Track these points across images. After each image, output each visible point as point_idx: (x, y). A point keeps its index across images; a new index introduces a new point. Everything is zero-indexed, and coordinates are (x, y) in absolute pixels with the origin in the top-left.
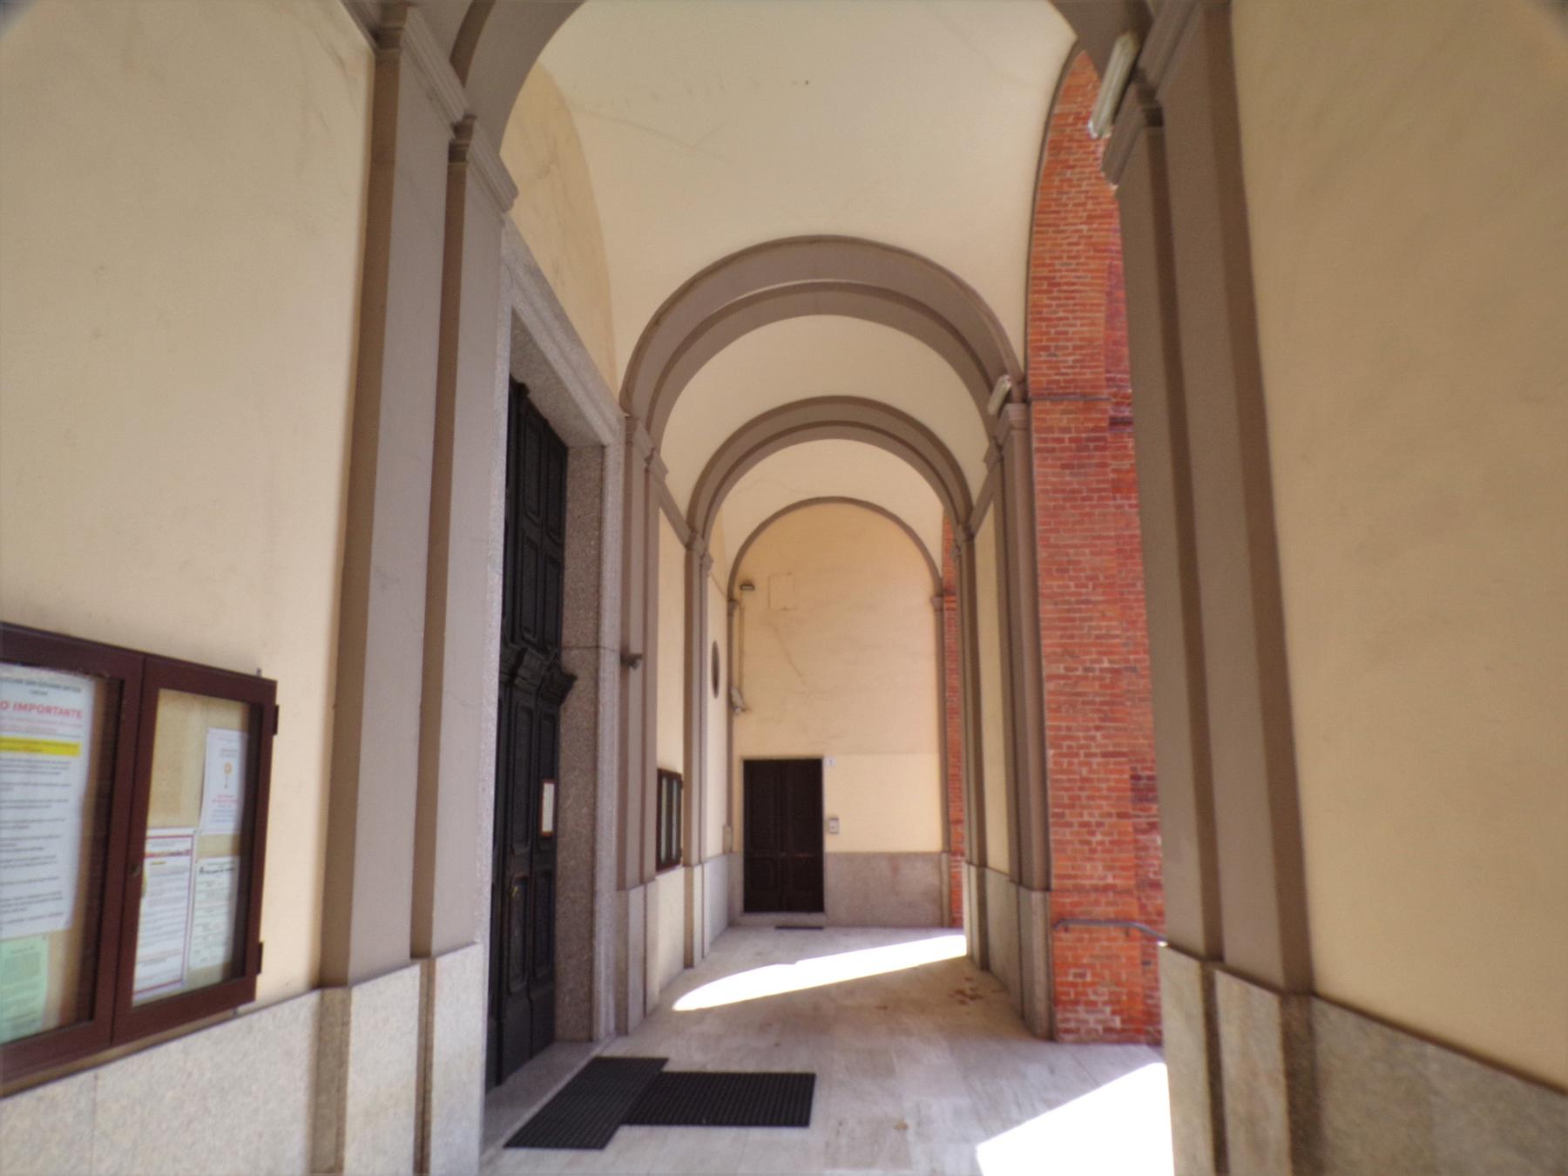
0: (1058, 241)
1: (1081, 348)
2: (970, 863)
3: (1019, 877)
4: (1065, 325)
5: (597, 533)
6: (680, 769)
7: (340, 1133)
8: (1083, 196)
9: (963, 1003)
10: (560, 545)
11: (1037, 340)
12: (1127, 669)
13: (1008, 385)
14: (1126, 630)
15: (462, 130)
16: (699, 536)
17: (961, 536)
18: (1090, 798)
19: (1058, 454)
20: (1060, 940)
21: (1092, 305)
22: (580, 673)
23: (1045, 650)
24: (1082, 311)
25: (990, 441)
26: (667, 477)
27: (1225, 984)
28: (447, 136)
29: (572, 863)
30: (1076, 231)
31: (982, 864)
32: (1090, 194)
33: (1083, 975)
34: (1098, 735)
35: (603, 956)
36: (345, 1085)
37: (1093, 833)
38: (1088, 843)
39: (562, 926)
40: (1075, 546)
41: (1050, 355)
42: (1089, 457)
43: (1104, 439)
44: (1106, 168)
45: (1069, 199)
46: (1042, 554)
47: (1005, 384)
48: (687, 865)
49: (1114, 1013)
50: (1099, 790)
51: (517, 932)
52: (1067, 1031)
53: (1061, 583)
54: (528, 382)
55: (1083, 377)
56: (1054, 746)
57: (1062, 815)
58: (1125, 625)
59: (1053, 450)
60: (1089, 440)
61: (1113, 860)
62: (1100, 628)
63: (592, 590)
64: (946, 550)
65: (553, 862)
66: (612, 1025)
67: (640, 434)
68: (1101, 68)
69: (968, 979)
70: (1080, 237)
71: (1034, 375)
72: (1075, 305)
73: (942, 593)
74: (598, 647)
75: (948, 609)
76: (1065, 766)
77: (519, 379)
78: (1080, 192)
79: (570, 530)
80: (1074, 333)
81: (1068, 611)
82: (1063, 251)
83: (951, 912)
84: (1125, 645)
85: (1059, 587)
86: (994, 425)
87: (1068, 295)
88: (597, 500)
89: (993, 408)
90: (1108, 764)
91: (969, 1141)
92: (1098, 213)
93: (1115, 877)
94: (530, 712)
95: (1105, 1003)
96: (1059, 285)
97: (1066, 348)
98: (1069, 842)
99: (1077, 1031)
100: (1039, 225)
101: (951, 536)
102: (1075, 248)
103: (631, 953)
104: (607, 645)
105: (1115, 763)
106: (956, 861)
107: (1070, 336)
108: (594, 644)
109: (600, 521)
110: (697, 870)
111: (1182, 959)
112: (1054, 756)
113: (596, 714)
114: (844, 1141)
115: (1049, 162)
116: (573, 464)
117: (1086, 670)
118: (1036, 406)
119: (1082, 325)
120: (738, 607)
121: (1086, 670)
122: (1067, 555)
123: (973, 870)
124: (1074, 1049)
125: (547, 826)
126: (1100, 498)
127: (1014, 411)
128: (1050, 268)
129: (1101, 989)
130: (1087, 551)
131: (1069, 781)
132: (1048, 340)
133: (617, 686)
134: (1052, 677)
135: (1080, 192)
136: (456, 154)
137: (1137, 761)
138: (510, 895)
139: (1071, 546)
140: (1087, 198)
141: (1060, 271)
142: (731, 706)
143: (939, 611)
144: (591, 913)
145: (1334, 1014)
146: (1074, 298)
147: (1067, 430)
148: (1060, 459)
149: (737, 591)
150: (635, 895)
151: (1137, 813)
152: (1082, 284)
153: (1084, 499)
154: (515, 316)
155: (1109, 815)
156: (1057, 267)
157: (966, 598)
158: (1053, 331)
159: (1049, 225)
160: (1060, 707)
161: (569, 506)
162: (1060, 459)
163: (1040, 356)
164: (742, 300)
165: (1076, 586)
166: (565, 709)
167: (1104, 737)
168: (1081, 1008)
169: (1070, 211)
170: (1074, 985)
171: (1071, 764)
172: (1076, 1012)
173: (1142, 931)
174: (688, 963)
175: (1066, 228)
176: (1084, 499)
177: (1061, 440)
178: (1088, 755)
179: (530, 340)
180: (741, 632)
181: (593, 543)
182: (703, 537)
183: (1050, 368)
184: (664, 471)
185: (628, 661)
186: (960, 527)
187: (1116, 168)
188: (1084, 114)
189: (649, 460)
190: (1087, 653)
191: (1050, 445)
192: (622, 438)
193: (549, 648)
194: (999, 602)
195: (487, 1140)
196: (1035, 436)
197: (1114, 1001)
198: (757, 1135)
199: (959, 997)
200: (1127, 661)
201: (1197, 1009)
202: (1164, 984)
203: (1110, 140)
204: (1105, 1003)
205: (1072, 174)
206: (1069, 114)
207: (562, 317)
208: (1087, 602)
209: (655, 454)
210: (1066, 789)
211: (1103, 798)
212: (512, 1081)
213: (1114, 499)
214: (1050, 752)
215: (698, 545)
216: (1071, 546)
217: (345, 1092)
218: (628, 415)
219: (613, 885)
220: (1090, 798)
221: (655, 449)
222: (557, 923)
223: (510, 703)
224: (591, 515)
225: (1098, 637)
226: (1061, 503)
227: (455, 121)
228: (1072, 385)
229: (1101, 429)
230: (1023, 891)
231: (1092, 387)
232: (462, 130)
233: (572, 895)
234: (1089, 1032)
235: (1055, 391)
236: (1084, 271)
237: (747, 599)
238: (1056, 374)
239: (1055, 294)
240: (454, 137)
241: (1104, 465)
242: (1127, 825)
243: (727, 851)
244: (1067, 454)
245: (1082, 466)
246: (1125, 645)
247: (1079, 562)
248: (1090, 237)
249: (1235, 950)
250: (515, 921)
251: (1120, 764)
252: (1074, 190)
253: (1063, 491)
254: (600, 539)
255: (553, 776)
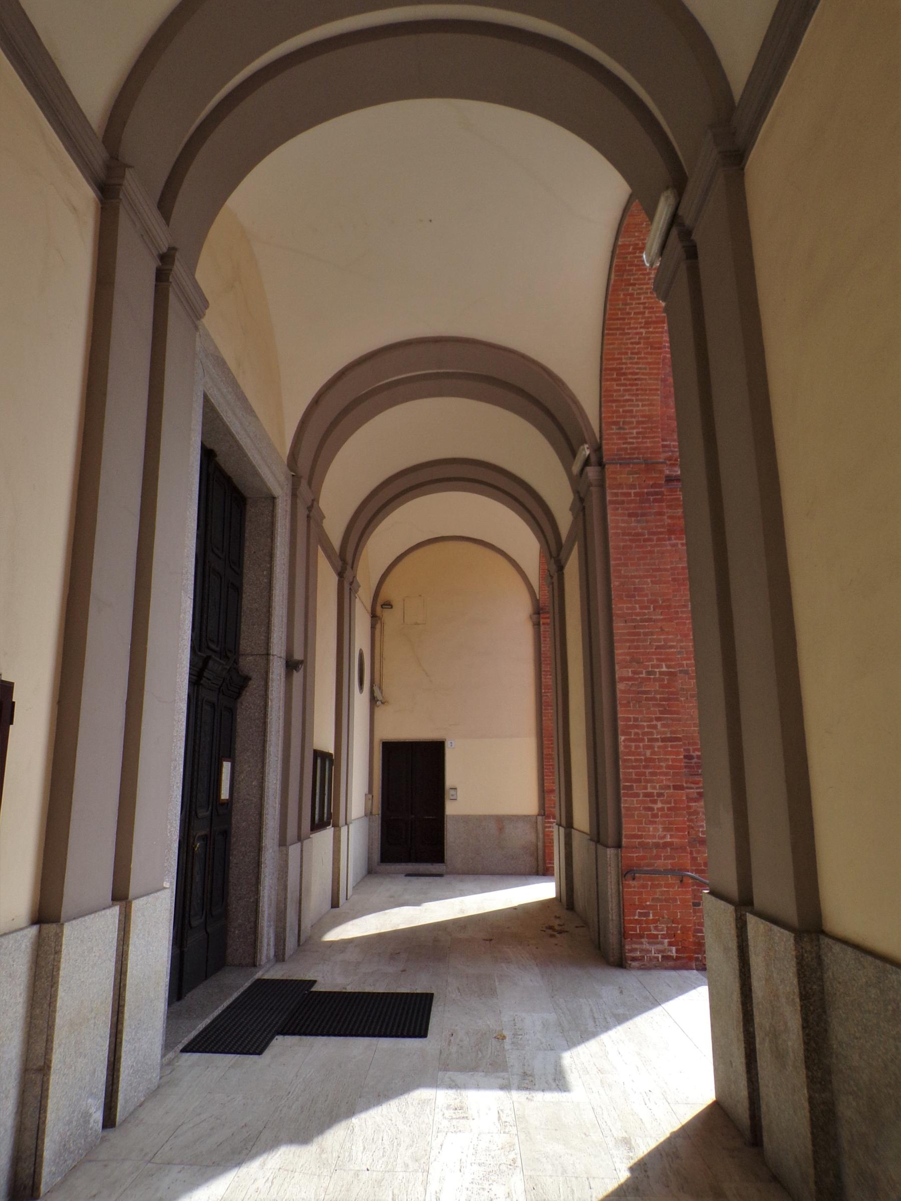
0: (624, 341)
1: (643, 422)
2: (560, 825)
3: (597, 837)
4: (630, 406)
5: (268, 565)
6: (331, 750)
7: (49, 1041)
8: (642, 306)
9: (552, 936)
10: (239, 574)
11: (609, 417)
12: (681, 672)
13: (588, 452)
14: (681, 641)
15: (166, 259)
16: (349, 567)
17: (553, 568)
18: (652, 774)
19: (626, 505)
20: (629, 886)
21: (650, 390)
22: (254, 675)
23: (618, 658)
24: (642, 395)
25: (574, 495)
26: (324, 521)
27: (754, 924)
28: (152, 265)
29: (244, 824)
30: (637, 334)
31: (569, 825)
32: (647, 305)
33: (647, 915)
34: (659, 724)
35: (266, 899)
36: (56, 1001)
37: (655, 802)
38: (651, 809)
39: (234, 873)
40: (639, 577)
41: (620, 428)
42: (650, 508)
43: (661, 493)
44: (656, 289)
45: (631, 309)
46: (615, 583)
47: (586, 451)
48: (336, 826)
49: (670, 944)
50: (660, 767)
51: (198, 878)
52: (634, 959)
53: (629, 605)
54: (216, 448)
55: (645, 445)
56: (624, 734)
57: (631, 787)
58: (679, 637)
59: (623, 502)
60: (648, 494)
61: (671, 823)
62: (659, 640)
63: (265, 610)
64: (541, 578)
65: (229, 823)
66: (272, 953)
67: (303, 487)
68: (651, 214)
69: (556, 917)
70: (640, 338)
71: (607, 444)
72: (637, 390)
73: (538, 611)
74: (268, 654)
75: (544, 624)
76: (633, 749)
77: (209, 446)
78: (639, 304)
79: (247, 562)
80: (637, 411)
81: (635, 627)
82: (628, 349)
83: (545, 863)
84: (679, 653)
85: (628, 608)
86: (577, 482)
87: (631, 382)
88: (269, 540)
89: (576, 468)
90: (666, 747)
91: (555, 1050)
92: (654, 319)
93: (671, 836)
94: (213, 705)
95: (664, 936)
96: (624, 374)
97: (632, 423)
98: (636, 809)
99: (641, 959)
100: (610, 329)
101: (546, 567)
102: (637, 346)
103: (289, 896)
104: (275, 653)
105: (672, 747)
106: (549, 822)
107: (634, 413)
108: (264, 652)
109: (271, 556)
110: (344, 830)
111: (722, 904)
112: (624, 741)
113: (266, 706)
114: (454, 1049)
115: (615, 281)
116: (251, 511)
117: (649, 673)
118: (609, 469)
119: (643, 406)
120: (379, 621)
121: (649, 673)
122: (634, 583)
123: (562, 830)
124: (640, 973)
125: (225, 794)
126: (659, 540)
127: (592, 472)
128: (618, 362)
129: (661, 926)
130: (649, 580)
131: (636, 760)
132: (617, 417)
133: (283, 684)
134: (623, 679)
135: (639, 304)
136: (162, 276)
137: (689, 744)
138: (194, 849)
139: (635, 577)
140: (645, 308)
141: (626, 364)
142: (373, 700)
143: (537, 625)
144: (258, 864)
145: (837, 948)
146: (637, 385)
147: (633, 486)
148: (627, 509)
149: (378, 609)
150: (294, 850)
151: (689, 785)
152: (643, 374)
153: (645, 540)
154: (206, 399)
155: (668, 787)
156: (624, 361)
157: (557, 617)
158: (621, 410)
159: (617, 329)
160: (629, 702)
161: (247, 544)
162: (627, 509)
163: (612, 429)
164: (384, 384)
165: (641, 608)
166: (242, 703)
167: (663, 726)
168: (644, 940)
169: (631, 318)
170: (638, 922)
171: (637, 747)
172: (642, 943)
173: (693, 878)
174: (335, 904)
175: (629, 331)
176: (645, 540)
177: (629, 494)
178: (650, 740)
179: (218, 417)
180: (382, 642)
181: (265, 573)
182: (352, 568)
183: (619, 439)
184: (323, 517)
185: (291, 666)
186: (553, 561)
187: (664, 288)
188: (641, 245)
189: (310, 508)
190: (650, 660)
191: (620, 498)
192: (289, 492)
193: (229, 654)
194: (583, 621)
195: (168, 1046)
196: (608, 491)
197: (671, 934)
198: (385, 1044)
199: (550, 932)
200: (682, 665)
201: (733, 945)
202: (707, 922)
203: (658, 269)
204: (664, 936)
205: (633, 289)
206: (629, 245)
207: (242, 398)
208: (649, 620)
209: (315, 503)
210: (634, 767)
211: (661, 774)
212: (189, 998)
213: (670, 539)
214: (622, 738)
215: (348, 573)
216: (635, 577)
217: (55, 1007)
218: (294, 474)
219: (276, 841)
220: (652, 774)
221: (315, 500)
222: (231, 872)
223: (197, 698)
224: (264, 551)
225: (658, 647)
226: (628, 543)
227: (161, 252)
228: (636, 452)
229: (660, 486)
230: (600, 847)
231: (652, 453)
232: (166, 259)
233: (243, 849)
234: (651, 959)
235: (623, 456)
236: (643, 364)
237: (387, 616)
238: (624, 443)
239: (623, 382)
240: (160, 264)
241: (661, 514)
242: (683, 795)
243: (369, 814)
244: (632, 505)
245: (643, 515)
246: (679, 653)
247: (642, 589)
248: (648, 338)
249: (762, 895)
250: (197, 868)
251: (675, 746)
252: (634, 302)
253: (629, 534)
254: (271, 570)
255: (231, 757)
